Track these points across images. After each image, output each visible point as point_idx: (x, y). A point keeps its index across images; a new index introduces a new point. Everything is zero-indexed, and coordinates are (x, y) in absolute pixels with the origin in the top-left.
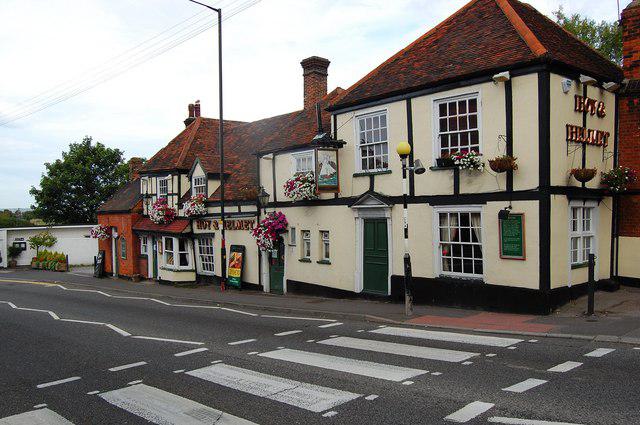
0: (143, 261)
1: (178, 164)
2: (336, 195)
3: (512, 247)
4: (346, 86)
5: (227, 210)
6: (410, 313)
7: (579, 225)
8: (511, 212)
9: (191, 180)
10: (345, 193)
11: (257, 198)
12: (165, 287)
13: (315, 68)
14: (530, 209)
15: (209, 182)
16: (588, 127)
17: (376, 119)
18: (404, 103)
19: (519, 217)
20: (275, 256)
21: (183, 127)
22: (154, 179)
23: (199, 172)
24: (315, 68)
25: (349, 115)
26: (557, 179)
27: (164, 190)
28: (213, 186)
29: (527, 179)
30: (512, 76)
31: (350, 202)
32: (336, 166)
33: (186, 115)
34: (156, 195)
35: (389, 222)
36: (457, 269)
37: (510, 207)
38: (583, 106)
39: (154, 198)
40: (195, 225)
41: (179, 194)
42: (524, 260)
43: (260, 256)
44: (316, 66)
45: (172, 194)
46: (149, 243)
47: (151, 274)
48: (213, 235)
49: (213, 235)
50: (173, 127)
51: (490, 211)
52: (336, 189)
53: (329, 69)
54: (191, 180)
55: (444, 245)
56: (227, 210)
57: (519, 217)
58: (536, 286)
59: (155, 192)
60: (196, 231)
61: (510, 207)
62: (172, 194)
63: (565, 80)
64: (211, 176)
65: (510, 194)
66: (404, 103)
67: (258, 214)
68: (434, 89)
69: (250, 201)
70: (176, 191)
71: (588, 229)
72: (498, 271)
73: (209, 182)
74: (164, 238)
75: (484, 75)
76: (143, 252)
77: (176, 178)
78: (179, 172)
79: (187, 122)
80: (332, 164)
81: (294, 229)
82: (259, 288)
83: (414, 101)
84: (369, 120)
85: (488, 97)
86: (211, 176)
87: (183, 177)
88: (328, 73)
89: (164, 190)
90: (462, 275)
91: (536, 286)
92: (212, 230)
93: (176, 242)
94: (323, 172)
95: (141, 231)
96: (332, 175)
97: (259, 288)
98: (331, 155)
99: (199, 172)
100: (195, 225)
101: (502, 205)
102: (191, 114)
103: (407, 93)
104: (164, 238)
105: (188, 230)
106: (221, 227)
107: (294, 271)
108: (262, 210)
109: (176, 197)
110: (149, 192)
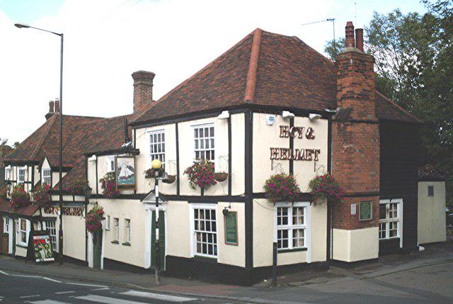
0: (5, 239)
1: (31, 158)
2: (135, 191)
3: (231, 239)
4: (21, 141)
5: (66, 198)
6: (158, 283)
7: (298, 220)
8: (229, 210)
9: (40, 171)
10: (140, 191)
11: (83, 189)
12: (272, 257)
13: (143, 80)
14: (239, 208)
15: (54, 174)
16: (295, 147)
17: (155, 135)
18: (174, 125)
19: (235, 214)
20: (371, 223)
21: (45, 120)
22: (15, 167)
23: (46, 165)
24: (143, 80)
25: (143, 130)
26: (258, 187)
27: (22, 178)
28: (56, 178)
29: (239, 189)
30: (230, 114)
31: (142, 197)
32: (133, 169)
33: (47, 111)
34: (16, 182)
35: (165, 214)
36: (205, 252)
37: (230, 207)
38: (291, 132)
39: (15, 184)
40: (43, 211)
41: (32, 182)
42: (237, 245)
43: (87, 237)
44: (143, 79)
45: (28, 182)
46: (11, 222)
47: (10, 251)
48: (56, 218)
49: (56, 218)
50: (36, 120)
51: (219, 208)
52: (134, 187)
53: (154, 80)
54: (40, 171)
55: (199, 234)
56: (66, 198)
57: (235, 214)
58: (243, 265)
59: (15, 179)
60: (44, 215)
61: (230, 207)
62: (28, 182)
63: (268, 116)
64: (54, 169)
65: (229, 198)
66: (174, 125)
67: (86, 203)
68: (187, 118)
69: (81, 193)
70: (30, 180)
71: (303, 223)
72: (231, 255)
73: (54, 174)
74: (20, 220)
75: (215, 112)
76: (5, 231)
77: (30, 168)
78: (32, 163)
79: (48, 116)
80: (130, 168)
81: (109, 217)
82: (85, 263)
83: (179, 124)
84: (155, 135)
85: (217, 123)
86: (54, 169)
87: (36, 167)
88: (154, 83)
89: (22, 178)
90: (207, 255)
91: (243, 265)
92: (55, 215)
93: (28, 223)
94: (122, 174)
95: (5, 213)
96: (130, 177)
97: (85, 263)
98: (131, 162)
99: (46, 165)
100: (43, 211)
101: (226, 204)
102: (51, 110)
103: (176, 119)
104: (20, 220)
105: (37, 213)
106: (59, 212)
107: (109, 251)
108: (91, 201)
109: (30, 185)
110: (11, 179)
